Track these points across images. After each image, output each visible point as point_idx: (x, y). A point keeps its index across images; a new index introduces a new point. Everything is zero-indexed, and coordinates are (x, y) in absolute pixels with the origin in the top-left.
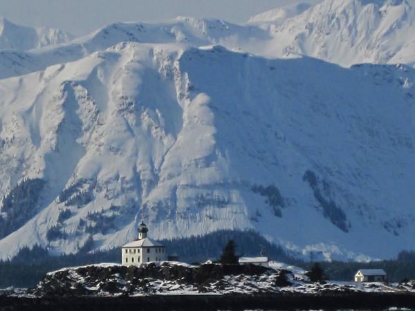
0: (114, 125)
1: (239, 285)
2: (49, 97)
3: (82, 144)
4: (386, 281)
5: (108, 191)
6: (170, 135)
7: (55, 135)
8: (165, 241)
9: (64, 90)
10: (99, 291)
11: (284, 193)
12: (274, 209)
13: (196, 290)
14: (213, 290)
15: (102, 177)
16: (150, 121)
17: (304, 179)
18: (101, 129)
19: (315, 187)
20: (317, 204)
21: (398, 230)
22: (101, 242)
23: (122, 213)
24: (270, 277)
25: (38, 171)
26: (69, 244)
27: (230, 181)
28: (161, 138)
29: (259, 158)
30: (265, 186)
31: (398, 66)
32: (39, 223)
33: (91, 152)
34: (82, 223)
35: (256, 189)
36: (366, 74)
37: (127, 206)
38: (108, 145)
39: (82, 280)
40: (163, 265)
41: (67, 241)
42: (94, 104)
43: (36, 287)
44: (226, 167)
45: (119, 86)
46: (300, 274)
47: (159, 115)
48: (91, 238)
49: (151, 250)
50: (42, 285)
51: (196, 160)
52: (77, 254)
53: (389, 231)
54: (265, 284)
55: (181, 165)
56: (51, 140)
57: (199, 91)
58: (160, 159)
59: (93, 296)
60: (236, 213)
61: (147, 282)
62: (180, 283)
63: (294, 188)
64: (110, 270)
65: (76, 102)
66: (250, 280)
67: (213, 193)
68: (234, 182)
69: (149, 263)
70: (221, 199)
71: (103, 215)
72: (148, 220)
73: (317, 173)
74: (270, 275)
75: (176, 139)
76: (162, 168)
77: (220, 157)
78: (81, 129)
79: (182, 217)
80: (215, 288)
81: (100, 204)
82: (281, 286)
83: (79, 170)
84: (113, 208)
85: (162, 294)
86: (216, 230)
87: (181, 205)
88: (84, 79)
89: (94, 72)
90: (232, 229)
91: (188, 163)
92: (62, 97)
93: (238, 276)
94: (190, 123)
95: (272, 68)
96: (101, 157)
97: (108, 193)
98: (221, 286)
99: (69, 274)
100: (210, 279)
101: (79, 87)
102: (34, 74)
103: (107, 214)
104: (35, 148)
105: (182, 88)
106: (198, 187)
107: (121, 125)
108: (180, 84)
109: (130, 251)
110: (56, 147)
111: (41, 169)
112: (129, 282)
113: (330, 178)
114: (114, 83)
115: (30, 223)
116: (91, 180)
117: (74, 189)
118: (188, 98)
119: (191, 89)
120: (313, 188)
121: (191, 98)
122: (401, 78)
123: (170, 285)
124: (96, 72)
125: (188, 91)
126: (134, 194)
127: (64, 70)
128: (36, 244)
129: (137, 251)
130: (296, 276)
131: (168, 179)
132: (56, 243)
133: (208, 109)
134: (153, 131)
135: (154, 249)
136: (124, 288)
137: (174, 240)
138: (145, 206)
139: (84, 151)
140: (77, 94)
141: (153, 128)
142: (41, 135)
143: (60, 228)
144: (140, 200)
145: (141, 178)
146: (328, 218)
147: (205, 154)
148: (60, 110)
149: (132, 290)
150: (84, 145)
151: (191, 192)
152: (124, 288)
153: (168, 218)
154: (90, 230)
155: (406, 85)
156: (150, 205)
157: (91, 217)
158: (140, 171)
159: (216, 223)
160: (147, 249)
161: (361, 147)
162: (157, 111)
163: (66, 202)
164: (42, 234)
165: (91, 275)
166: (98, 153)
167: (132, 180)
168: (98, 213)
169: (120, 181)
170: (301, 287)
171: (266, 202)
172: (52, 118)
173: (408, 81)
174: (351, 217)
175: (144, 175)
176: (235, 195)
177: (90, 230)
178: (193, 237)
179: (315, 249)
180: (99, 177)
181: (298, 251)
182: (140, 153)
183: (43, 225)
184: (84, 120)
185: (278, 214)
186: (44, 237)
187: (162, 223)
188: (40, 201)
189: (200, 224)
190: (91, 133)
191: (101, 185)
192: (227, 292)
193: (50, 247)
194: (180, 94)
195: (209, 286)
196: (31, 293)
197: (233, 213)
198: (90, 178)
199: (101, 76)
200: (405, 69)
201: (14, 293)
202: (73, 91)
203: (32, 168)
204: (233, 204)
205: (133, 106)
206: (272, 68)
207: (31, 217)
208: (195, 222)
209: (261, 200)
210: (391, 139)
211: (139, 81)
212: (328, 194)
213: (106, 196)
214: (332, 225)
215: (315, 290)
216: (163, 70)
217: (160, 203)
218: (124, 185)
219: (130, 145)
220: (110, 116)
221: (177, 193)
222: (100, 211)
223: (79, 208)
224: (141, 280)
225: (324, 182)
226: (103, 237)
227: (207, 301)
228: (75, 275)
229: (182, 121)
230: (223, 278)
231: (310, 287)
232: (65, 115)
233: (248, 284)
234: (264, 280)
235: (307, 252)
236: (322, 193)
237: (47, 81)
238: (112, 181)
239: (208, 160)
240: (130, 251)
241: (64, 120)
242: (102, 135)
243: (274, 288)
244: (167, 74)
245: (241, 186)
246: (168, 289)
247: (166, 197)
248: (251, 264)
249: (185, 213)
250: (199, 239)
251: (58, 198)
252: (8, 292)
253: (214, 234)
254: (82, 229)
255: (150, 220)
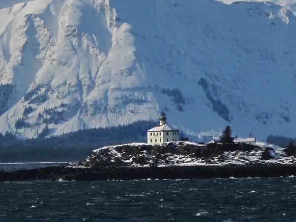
0: (63, 45)
1: (235, 159)
2: (16, 26)
3: (40, 59)
5: (59, 93)
6: (103, 53)
7: (20, 53)
8: (100, 129)
9: (27, 21)
10: (132, 163)
11: (185, 94)
12: (178, 106)
13: (204, 162)
14: (216, 162)
15: (55, 83)
16: (88, 43)
17: (199, 84)
18: (53, 49)
19: (207, 90)
20: (208, 102)
21: (266, 120)
22: (54, 130)
23: (69, 108)
24: (258, 152)
25: (8, 79)
26: (31, 131)
27: (146, 86)
28: (96, 55)
29: (166, 69)
30: (171, 89)
31: (265, 3)
32: (9, 116)
33: (46, 65)
34: (40, 116)
35: (164, 92)
36: (242, 9)
37: (73, 104)
38: (58, 60)
39: (119, 155)
40: (179, 144)
41: (30, 129)
42: (48, 30)
43: (85, 161)
44: (143, 76)
45: (67, 18)
46: (279, 150)
47: (95, 38)
48: (47, 127)
49: (169, 133)
50: (90, 159)
51: (121, 71)
52: (37, 138)
53: (259, 121)
54: (254, 157)
55: (110, 74)
56: (18, 56)
57: (123, 21)
58: (96, 70)
59: (128, 167)
60: (150, 108)
61: (167, 156)
62: (191, 157)
63: (192, 91)
64: (140, 148)
65: (36, 29)
66: (243, 155)
67: (134, 94)
68: (149, 87)
69: (168, 143)
70: (140, 98)
71: (56, 110)
72: (87, 114)
73: (208, 80)
74: (258, 151)
75: (107, 56)
76: (98, 76)
77: (139, 68)
78: (39, 49)
79: (112, 111)
80: (218, 161)
81: (53, 103)
82: (266, 159)
83: (38, 78)
84: (62, 105)
85: (179, 165)
86: (136, 121)
87: (111, 103)
88: (41, 12)
89: (48, 7)
90: (148, 120)
91: (116, 73)
92: (25, 27)
93: (234, 152)
94: (117, 44)
95: (175, 5)
96: (53, 68)
97: (59, 95)
98: (222, 160)
99: (109, 151)
100: (214, 154)
101: (38, 19)
102: (4, 9)
103: (58, 110)
104: (6, 63)
105: (111, 19)
106: (123, 90)
107: (68, 45)
108: (110, 16)
109: (154, 134)
110: (22, 62)
111: (11, 77)
112: (154, 156)
113: (217, 84)
114: (62, 15)
115: (4, 115)
116: (46, 85)
117: (34, 92)
118: (116, 26)
119: (117, 19)
120: (205, 91)
121: (118, 26)
122: (267, 12)
123: (184, 159)
124: (50, 8)
125: (116, 21)
126: (77, 95)
127: (27, 6)
128: (8, 131)
129: (159, 134)
130: (277, 152)
131: (102, 84)
132: (21, 131)
133: (130, 34)
134: (91, 50)
135: (171, 133)
136: (151, 161)
137: (107, 128)
138: (85, 104)
139: (41, 65)
140: (36, 24)
141: (91, 48)
142: (11, 53)
143: (25, 119)
144: (82, 99)
145: (82, 83)
146: (216, 112)
147: (128, 66)
148: (24, 36)
149: (157, 162)
150: (41, 60)
151: (118, 94)
152: (151, 161)
153: (102, 113)
154: (46, 121)
155: (271, 16)
156: (89, 103)
157: (47, 112)
158: (82, 79)
159: (136, 115)
160: (167, 133)
161: (239, 61)
162: (94, 36)
163: (29, 101)
164: (11, 124)
165: (126, 152)
166: (51, 66)
167: (76, 85)
168: (52, 109)
169: (67, 86)
170: (280, 160)
171: (172, 101)
172: (18, 41)
173: (273, 14)
175: (85, 81)
176: (150, 96)
177: (46, 121)
178: (120, 126)
179: (207, 134)
180: (52, 83)
181: (195, 135)
182: (81, 67)
183: (13, 118)
184: (41, 43)
185: (180, 109)
186: (13, 126)
187: (98, 116)
188: (10, 101)
189: (125, 116)
190: (46, 51)
191: (54, 89)
192: (227, 163)
193: (17, 133)
194: (110, 23)
195: (213, 159)
196: (82, 165)
197: (148, 108)
198: (46, 83)
199: (53, 11)
200: (270, 5)
201: (69, 165)
202: (33, 21)
203: (4, 76)
204: (148, 102)
205: (76, 32)
206: (175, 5)
207: (4, 112)
208: (121, 115)
209: (168, 99)
210: (261, 56)
211: (80, 14)
212: (216, 95)
213: (57, 97)
214: (219, 117)
215: (291, 162)
216: (97, 6)
217: (96, 101)
218: (70, 89)
219: (74, 60)
220: (60, 40)
221: (108, 94)
222: (53, 107)
223: (38, 105)
224: (163, 155)
226: (56, 126)
227: (215, 170)
228: (114, 152)
229: (111, 43)
230: (224, 154)
231: (287, 159)
232: (27, 39)
233: (242, 158)
234: (253, 155)
235: (202, 136)
236: (212, 94)
237: (14, 14)
238: (61, 86)
239: (130, 71)
240: (154, 134)
241: (26, 43)
242: (54, 52)
243: (261, 161)
244: (100, 10)
245: (156, 89)
246: (183, 162)
247: (101, 97)
248: (244, 144)
249: (114, 109)
250: (124, 128)
251: (23, 98)
252: (65, 164)
253: (135, 123)
254: (41, 120)
255: (89, 114)
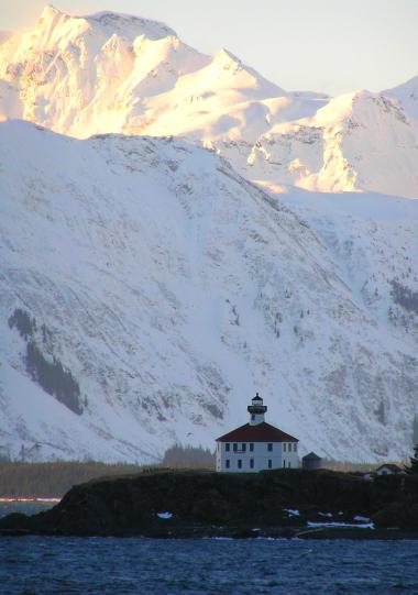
4: (291, 118)
21: (165, 412)
120: (26, 339)
174: (88, 387)
212: (50, 350)
225: (44, 328)
